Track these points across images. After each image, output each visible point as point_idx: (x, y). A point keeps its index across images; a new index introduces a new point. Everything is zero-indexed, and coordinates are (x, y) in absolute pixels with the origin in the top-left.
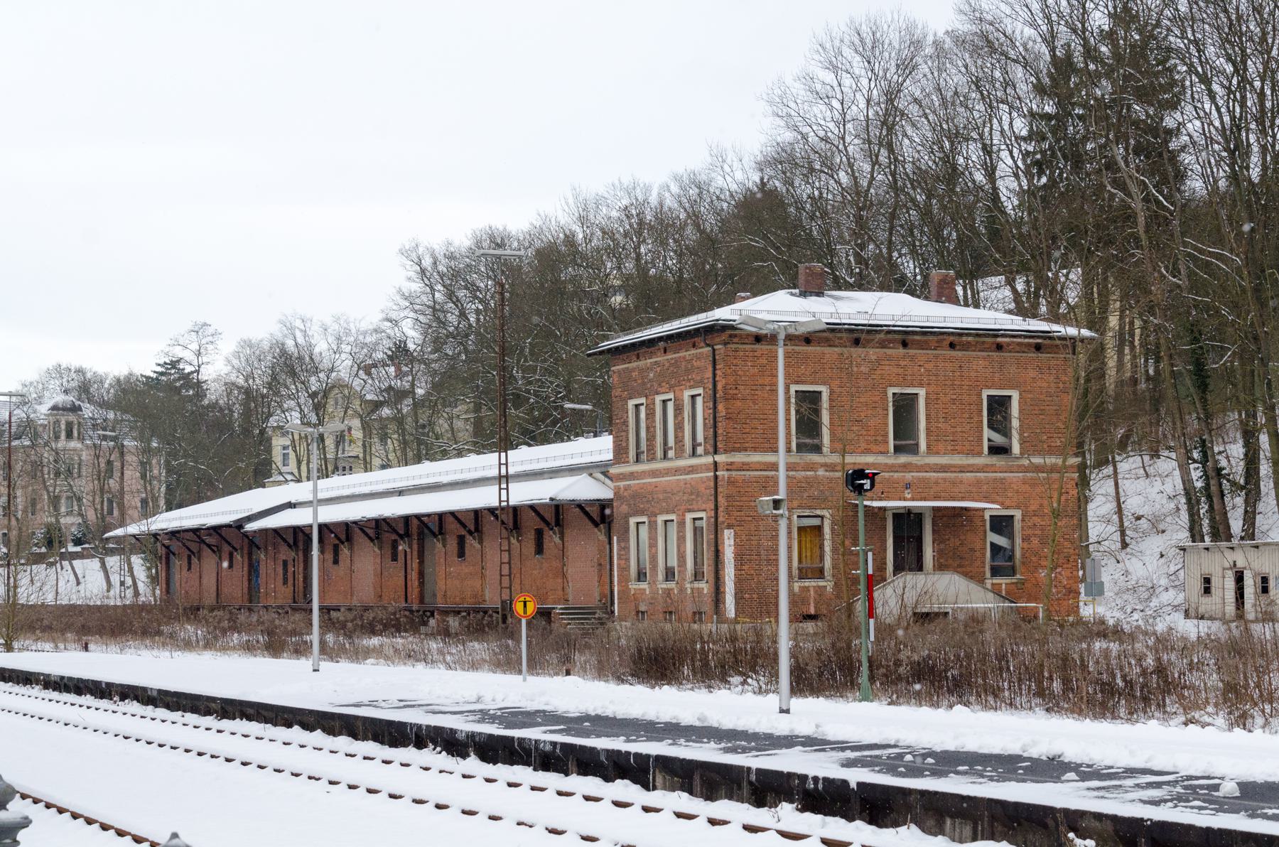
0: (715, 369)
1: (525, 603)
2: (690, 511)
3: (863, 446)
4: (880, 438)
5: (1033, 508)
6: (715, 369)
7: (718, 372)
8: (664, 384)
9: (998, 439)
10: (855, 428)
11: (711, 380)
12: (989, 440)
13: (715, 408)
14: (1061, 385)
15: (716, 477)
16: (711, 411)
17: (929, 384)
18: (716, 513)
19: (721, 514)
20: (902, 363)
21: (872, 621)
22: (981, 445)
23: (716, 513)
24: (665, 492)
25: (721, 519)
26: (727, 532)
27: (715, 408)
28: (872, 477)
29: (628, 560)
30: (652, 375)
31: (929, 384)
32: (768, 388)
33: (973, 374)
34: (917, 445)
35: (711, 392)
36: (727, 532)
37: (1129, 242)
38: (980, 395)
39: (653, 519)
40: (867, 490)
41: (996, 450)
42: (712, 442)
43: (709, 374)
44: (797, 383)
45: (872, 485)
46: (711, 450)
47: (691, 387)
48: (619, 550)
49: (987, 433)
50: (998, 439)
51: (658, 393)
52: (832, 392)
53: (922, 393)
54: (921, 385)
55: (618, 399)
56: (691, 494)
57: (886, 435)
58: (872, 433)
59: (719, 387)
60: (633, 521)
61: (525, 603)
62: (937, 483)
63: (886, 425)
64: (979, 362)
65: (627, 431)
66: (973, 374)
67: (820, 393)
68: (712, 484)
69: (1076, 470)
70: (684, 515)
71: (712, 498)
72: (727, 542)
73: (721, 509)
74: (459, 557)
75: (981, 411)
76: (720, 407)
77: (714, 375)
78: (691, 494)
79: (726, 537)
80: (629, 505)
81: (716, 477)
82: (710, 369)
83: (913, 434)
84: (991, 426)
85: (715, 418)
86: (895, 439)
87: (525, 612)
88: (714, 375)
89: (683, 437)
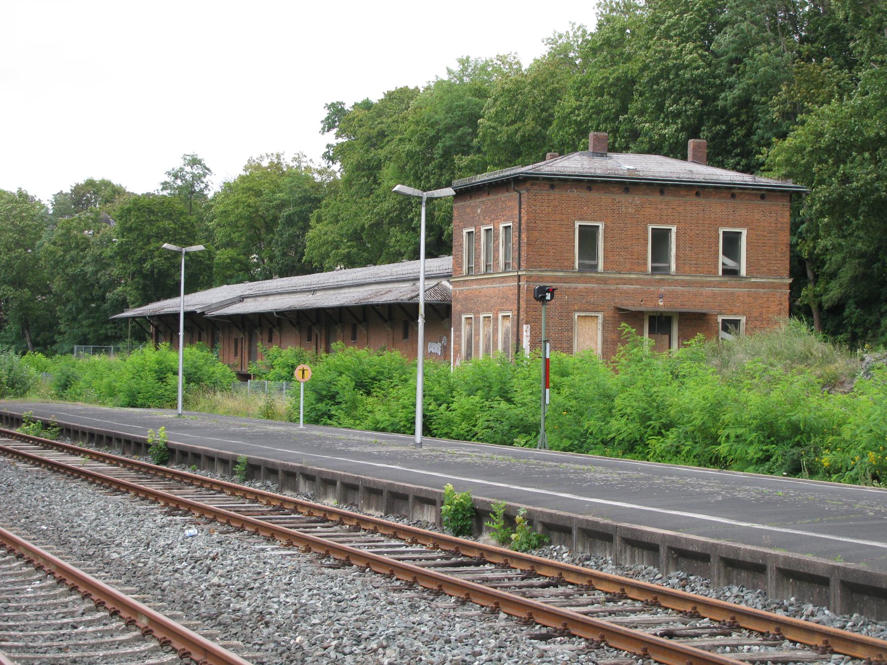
0: (520, 208)
1: (303, 371)
2: (502, 310)
3: (628, 266)
4: (641, 261)
5: (754, 314)
6: (520, 208)
7: (523, 211)
8: (487, 218)
9: (731, 263)
10: (622, 253)
11: (518, 216)
12: (723, 264)
13: (520, 236)
14: (779, 225)
15: (519, 286)
16: (517, 238)
17: (679, 222)
18: (519, 313)
19: (522, 313)
20: (659, 206)
21: (547, 390)
22: (717, 267)
23: (519, 313)
24: (486, 296)
25: (521, 317)
26: (525, 326)
27: (520, 236)
28: (552, 291)
29: (460, 345)
30: (479, 211)
31: (679, 222)
32: (559, 222)
33: (713, 216)
34: (669, 267)
35: (517, 225)
36: (525, 326)
37: (716, 122)
38: (717, 231)
39: (477, 315)
40: (548, 300)
41: (731, 273)
42: (517, 261)
43: (517, 212)
44: (581, 219)
45: (552, 297)
46: (516, 267)
47: (505, 220)
48: (455, 337)
49: (721, 258)
50: (731, 263)
51: (483, 224)
52: (606, 227)
53: (601, 226)
54: (673, 223)
55: (457, 227)
56: (503, 298)
57: (646, 259)
58: (635, 257)
59: (523, 221)
60: (464, 317)
61: (303, 371)
62: (682, 294)
63: (646, 251)
64: (716, 207)
65: (462, 251)
66: (713, 216)
67: (598, 227)
68: (516, 291)
69: (788, 287)
70: (497, 314)
71: (516, 301)
72: (525, 334)
73: (522, 310)
74: (352, 340)
75: (718, 242)
76: (524, 236)
77: (520, 213)
78: (503, 298)
79: (524, 330)
80: (462, 306)
81: (519, 286)
82: (517, 207)
83: (666, 259)
84: (725, 253)
85: (519, 243)
86: (652, 262)
87: (303, 377)
88: (520, 213)
89: (499, 256)
